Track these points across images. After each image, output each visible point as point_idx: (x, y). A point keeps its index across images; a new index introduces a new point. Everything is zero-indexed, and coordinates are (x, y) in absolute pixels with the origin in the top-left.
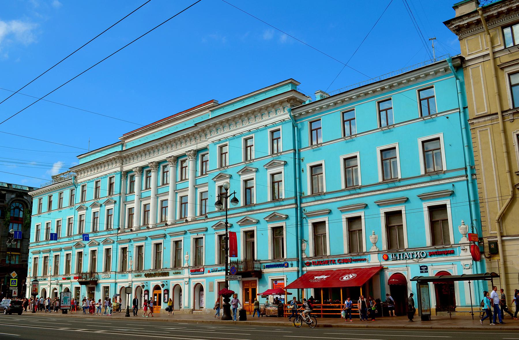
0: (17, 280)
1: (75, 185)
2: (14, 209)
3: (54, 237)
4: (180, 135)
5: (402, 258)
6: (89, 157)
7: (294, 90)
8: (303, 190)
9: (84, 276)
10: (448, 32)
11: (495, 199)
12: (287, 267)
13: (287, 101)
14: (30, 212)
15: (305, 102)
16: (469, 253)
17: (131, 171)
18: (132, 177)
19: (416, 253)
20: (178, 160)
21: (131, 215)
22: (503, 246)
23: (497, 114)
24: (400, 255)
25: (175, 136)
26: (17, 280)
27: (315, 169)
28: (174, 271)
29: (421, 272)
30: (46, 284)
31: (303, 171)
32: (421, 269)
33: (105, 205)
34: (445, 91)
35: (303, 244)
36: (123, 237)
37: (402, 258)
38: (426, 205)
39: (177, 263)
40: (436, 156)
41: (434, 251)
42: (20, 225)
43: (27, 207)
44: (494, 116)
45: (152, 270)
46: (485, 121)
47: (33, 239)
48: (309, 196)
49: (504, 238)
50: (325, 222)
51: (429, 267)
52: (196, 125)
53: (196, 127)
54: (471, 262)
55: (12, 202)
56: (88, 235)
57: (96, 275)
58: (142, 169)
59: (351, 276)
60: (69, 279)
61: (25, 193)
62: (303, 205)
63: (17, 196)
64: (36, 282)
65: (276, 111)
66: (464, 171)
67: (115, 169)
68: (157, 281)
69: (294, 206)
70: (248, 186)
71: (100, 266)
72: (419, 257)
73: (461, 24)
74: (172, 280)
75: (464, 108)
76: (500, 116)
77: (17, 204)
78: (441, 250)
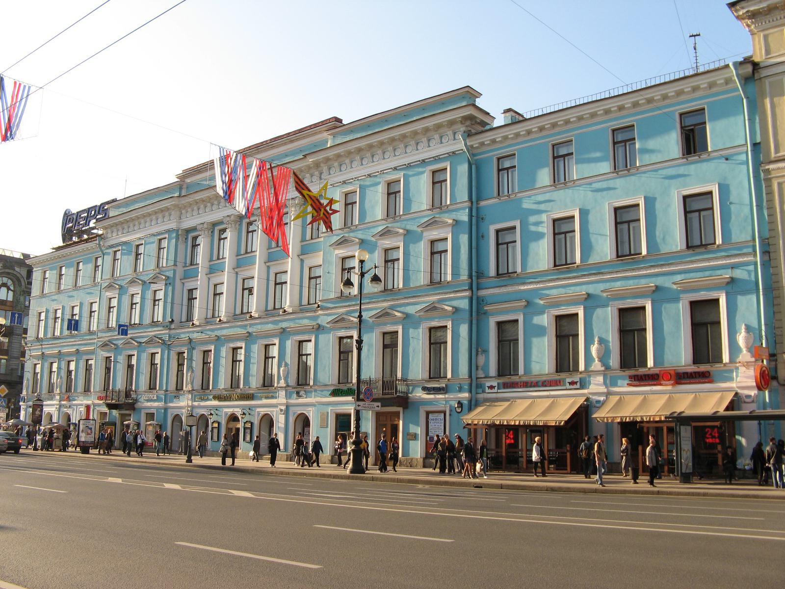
17: (194, 229)
21: (191, 299)
52: (305, 156)
62: (483, 293)
68: (235, 407)
69: (467, 294)
74: (262, 406)
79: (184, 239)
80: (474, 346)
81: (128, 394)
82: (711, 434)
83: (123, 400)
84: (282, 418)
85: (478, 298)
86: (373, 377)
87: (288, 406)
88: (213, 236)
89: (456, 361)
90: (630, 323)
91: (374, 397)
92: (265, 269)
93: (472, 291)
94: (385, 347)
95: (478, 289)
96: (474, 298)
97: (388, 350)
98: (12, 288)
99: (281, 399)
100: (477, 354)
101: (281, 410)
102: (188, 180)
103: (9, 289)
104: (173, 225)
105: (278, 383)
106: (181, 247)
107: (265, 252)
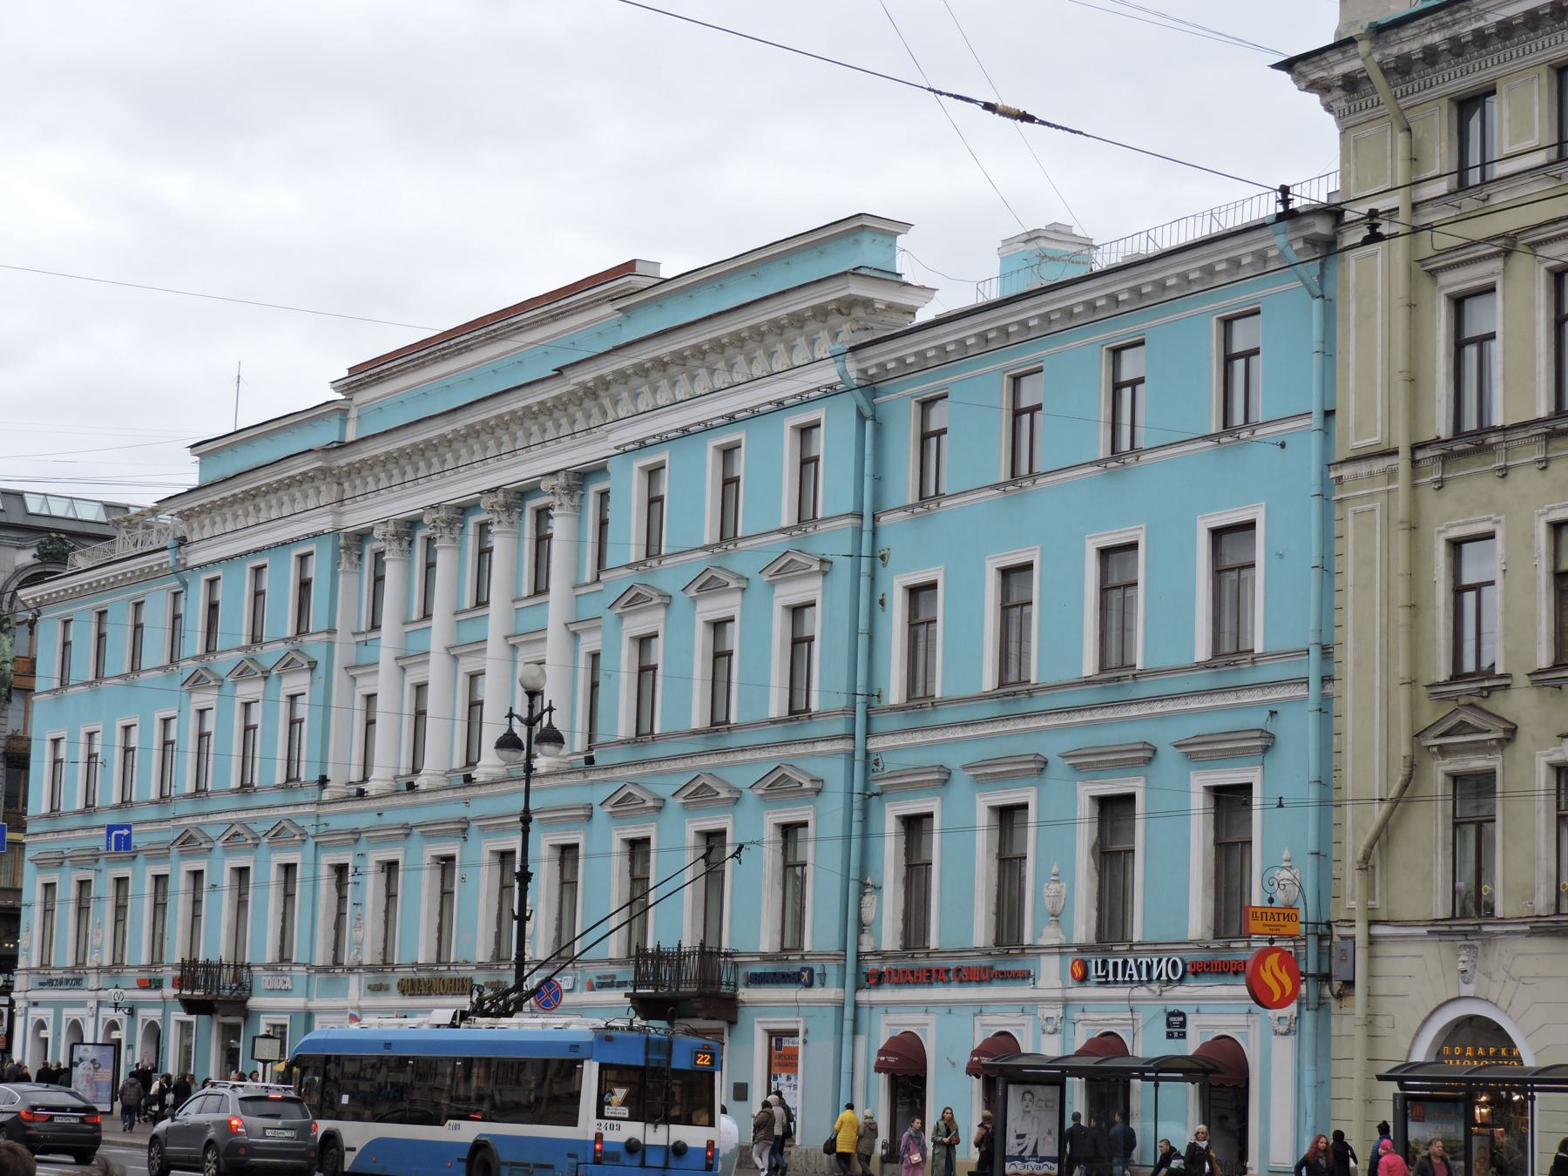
1: (181, 571)
4: (516, 403)
5: (1120, 978)
8: (879, 683)
12: (810, 985)
13: (839, 311)
15: (912, 312)
18: (543, 514)
19: (1159, 962)
22: (1371, 957)
27: (919, 593)
29: (1170, 1036)
30: (82, 1004)
31: (882, 602)
32: (1169, 1024)
33: (235, 683)
35: (867, 899)
38: (1201, 780)
44: (1379, 465)
45: (481, 966)
49: (1378, 930)
51: (1189, 1018)
52: (560, 371)
53: (559, 381)
58: (409, 527)
62: (874, 744)
67: (313, 519)
72: (1164, 977)
75: (1329, 414)
76: (1402, 462)
79: (354, 558)
82: (492, 1097)
85: (867, 754)
86: (687, 945)
104: (324, 522)
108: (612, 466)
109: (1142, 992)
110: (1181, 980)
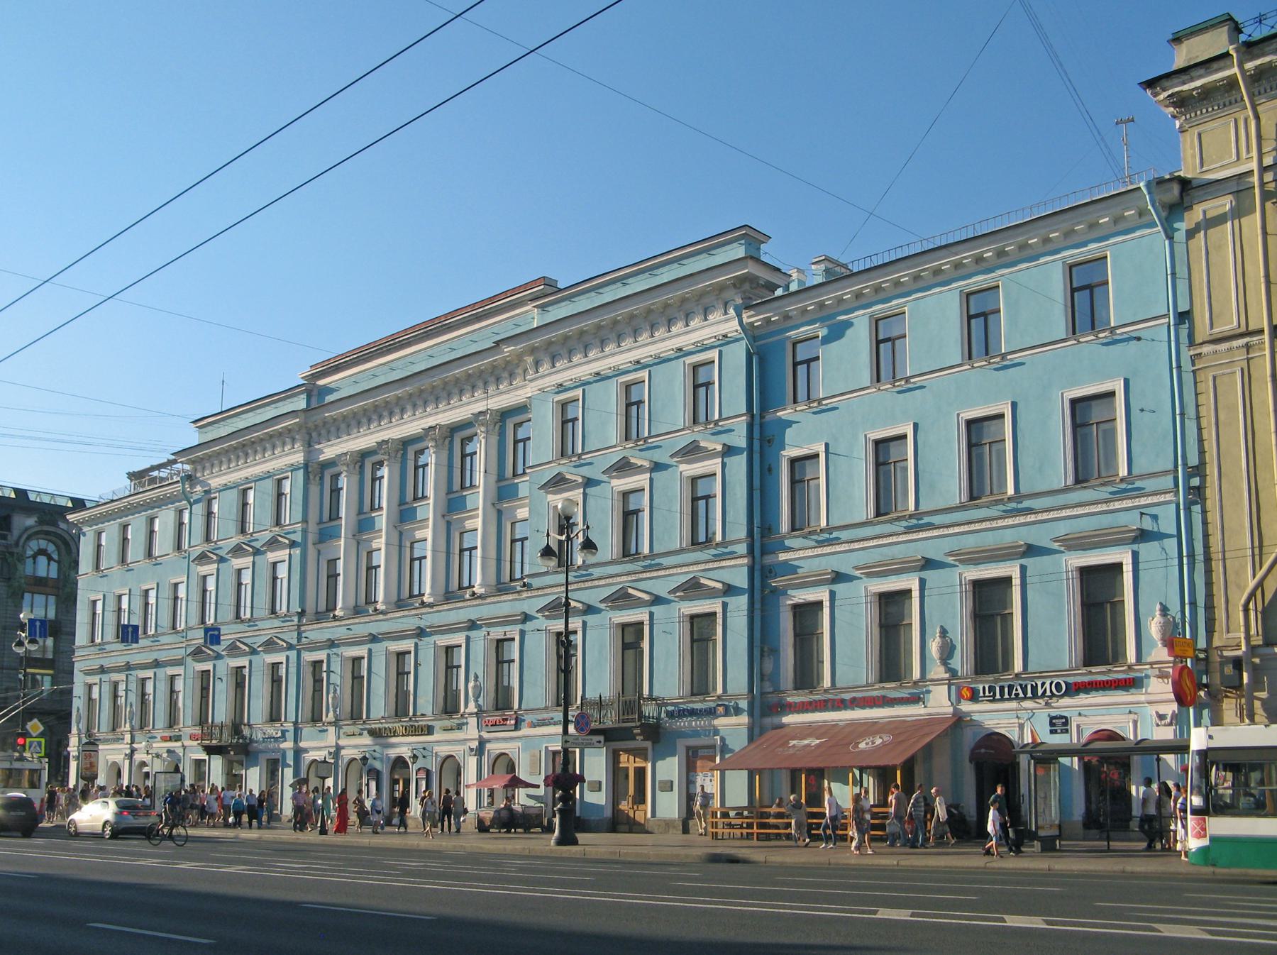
0: (43, 740)
2: (34, 557)
3: (128, 634)
5: (1006, 696)
6: (251, 414)
7: (752, 258)
9: (217, 732)
10: (1158, 104)
11: (1240, 553)
13: (734, 286)
14: (76, 564)
16: (1169, 687)
18: (336, 477)
19: (1043, 684)
20: (452, 437)
23: (1261, 331)
24: (1002, 689)
25: (608, 316)
26: (43, 740)
28: (447, 723)
29: (1052, 732)
31: (770, 470)
32: (1052, 724)
34: (1137, 266)
36: (317, 633)
37: (1006, 696)
39: (449, 706)
40: (1104, 439)
41: (1086, 679)
42: (52, 599)
43: (69, 551)
46: (1231, 349)
47: (81, 637)
48: (84, 647)
50: (910, 591)
52: (498, 343)
54: (1174, 707)
55: (28, 538)
56: (219, 630)
57: (246, 731)
59: (878, 741)
60: (178, 738)
61: (61, 512)
62: (769, 560)
63: (41, 522)
64: (91, 748)
65: (485, 383)
66: (1170, 478)
69: (745, 561)
70: (632, 507)
71: (257, 708)
72: (1048, 693)
73: (1186, 87)
74: (442, 743)
77: (43, 544)
78: (1104, 678)
80: (757, 642)
81: (236, 728)
83: (227, 739)
84: (472, 763)
85: (763, 567)
87: (482, 743)
88: (361, 473)
89: (732, 670)
90: (988, 601)
91: (594, 725)
92: (395, 535)
93: (753, 557)
94: (625, 647)
95: (763, 553)
96: (757, 567)
97: (630, 653)
98: (55, 556)
99: (472, 731)
100: (762, 656)
101: (472, 750)
102: (321, 382)
103: (50, 559)
105: (466, 706)
106: (314, 490)
107: (395, 508)
108: (535, 403)
109: (1028, 704)
110: (1062, 696)
